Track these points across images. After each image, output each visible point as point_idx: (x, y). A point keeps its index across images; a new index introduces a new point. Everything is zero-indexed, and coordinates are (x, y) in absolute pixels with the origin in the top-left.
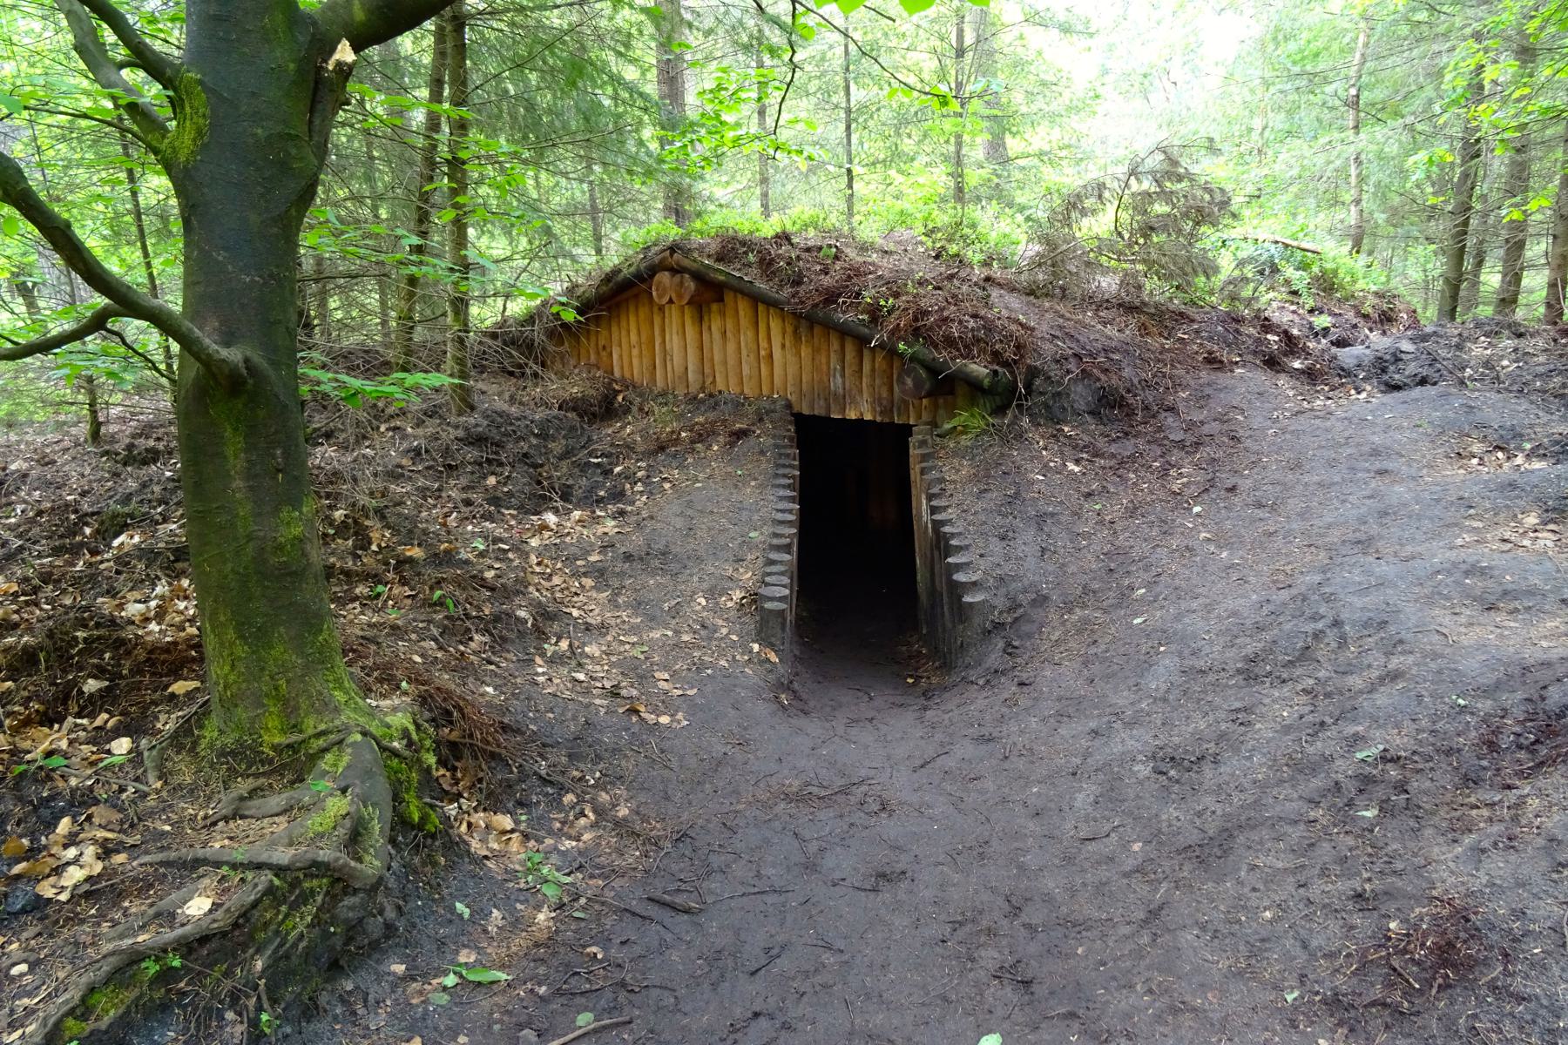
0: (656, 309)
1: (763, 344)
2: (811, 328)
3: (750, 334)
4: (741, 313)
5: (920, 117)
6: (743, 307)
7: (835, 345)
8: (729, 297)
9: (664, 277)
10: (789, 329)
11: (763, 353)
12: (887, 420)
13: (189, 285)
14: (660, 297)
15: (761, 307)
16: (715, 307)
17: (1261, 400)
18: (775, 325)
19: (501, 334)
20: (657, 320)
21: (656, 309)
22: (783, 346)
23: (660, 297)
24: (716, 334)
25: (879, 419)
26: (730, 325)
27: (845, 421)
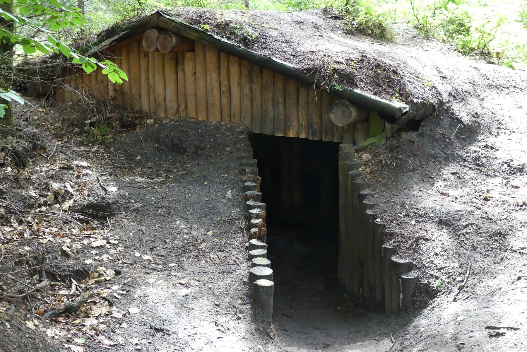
0: (142, 55)
1: (224, 82)
2: (261, 71)
3: (214, 75)
4: (208, 60)
5: (241, 263)
6: (211, 57)
7: (280, 85)
8: (198, 49)
9: (153, 33)
10: (245, 72)
11: (223, 89)
12: (317, 138)
13: (356, 93)
14: (149, 47)
15: (223, 57)
16: (188, 55)
17: (147, 60)
18: (234, 69)
19: (26, 68)
20: (143, 63)
21: (142, 55)
22: (239, 84)
23: (149, 47)
24: (189, 76)
25: (310, 138)
26: (199, 68)
27: (286, 139)
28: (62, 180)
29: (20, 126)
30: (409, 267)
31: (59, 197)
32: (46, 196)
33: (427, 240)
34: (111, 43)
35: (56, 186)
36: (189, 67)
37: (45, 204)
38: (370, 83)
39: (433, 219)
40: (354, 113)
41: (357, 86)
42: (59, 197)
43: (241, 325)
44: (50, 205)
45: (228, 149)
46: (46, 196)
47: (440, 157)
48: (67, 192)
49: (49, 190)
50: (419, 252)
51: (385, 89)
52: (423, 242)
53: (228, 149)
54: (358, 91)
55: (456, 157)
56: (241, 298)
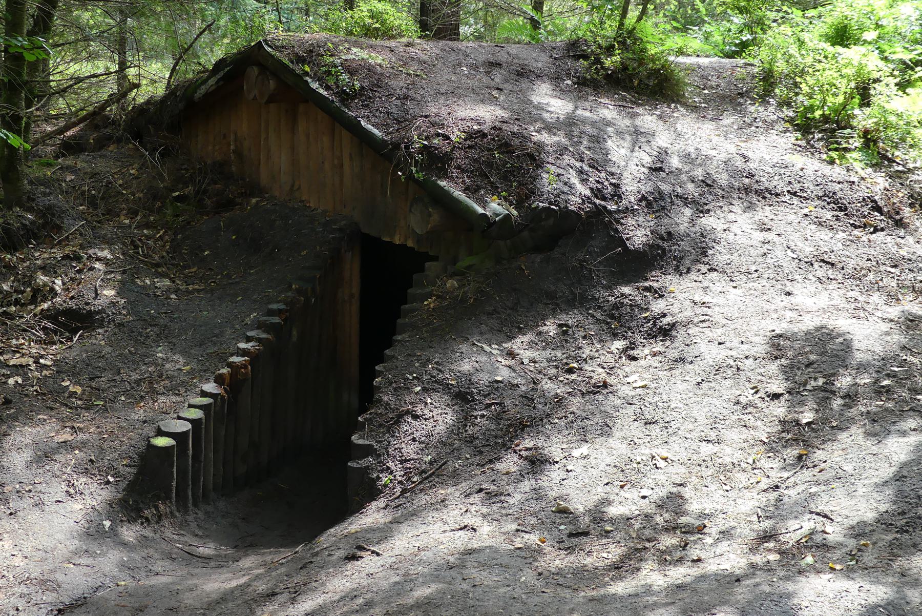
27: (391, 244)
28: (55, 272)
29: (34, 194)
30: (367, 451)
31: (39, 293)
32: (22, 292)
33: (416, 417)
34: (217, 83)
35: (42, 278)
36: (302, 126)
37: (17, 302)
38: (472, 172)
39: (450, 389)
40: (436, 217)
41: (446, 176)
42: (39, 293)
43: (103, 493)
44: (22, 305)
45: (304, 253)
46: (22, 292)
47: (561, 297)
48: (52, 290)
49: (30, 285)
50: (394, 432)
51: (492, 183)
52: (410, 419)
53: (304, 253)
54: (443, 183)
55: (588, 301)
56: (130, 457)
